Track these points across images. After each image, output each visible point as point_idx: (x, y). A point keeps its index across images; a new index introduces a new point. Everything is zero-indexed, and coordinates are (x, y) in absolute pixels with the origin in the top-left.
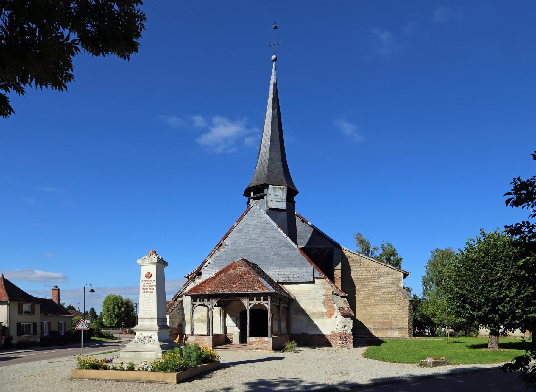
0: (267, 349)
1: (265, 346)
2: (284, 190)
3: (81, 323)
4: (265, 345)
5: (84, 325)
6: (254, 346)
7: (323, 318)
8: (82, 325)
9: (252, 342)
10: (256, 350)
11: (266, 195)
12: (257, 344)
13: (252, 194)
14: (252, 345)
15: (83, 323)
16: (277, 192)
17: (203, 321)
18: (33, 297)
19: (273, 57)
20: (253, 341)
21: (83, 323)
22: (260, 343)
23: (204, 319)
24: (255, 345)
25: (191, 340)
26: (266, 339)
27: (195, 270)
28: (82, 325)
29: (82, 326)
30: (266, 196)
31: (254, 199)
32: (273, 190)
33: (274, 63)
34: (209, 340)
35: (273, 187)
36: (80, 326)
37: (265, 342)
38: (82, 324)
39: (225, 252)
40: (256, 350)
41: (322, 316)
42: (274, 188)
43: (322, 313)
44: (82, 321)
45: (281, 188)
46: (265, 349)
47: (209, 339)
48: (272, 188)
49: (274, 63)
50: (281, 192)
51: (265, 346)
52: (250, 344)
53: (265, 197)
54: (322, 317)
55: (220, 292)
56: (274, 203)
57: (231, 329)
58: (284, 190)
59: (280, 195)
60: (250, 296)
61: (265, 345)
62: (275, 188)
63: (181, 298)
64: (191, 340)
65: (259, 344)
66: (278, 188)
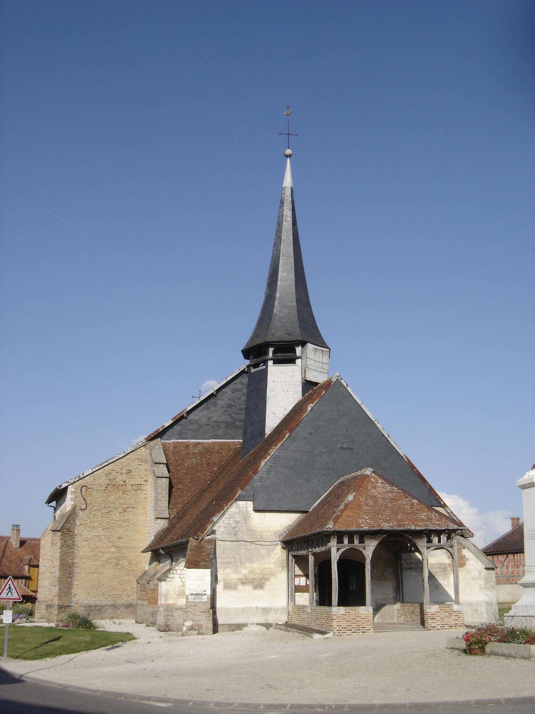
0: (457, 624)
1: (454, 620)
2: (326, 353)
3: (8, 586)
4: (454, 617)
5: (14, 591)
6: (439, 620)
7: (446, 573)
8: (10, 590)
9: (435, 614)
10: (441, 627)
11: (300, 358)
12: (442, 616)
13: (271, 350)
14: (435, 618)
15: (12, 586)
16: (318, 355)
17: (253, 581)
18: (524, 543)
19: (289, 152)
20: (437, 612)
21: (12, 586)
22: (447, 614)
23: (256, 577)
24: (438, 618)
25: (336, 615)
26: (361, 610)
27: (83, 474)
28: (10, 590)
29: (10, 594)
30: (300, 360)
31: (277, 362)
32: (313, 352)
33: (288, 160)
34: (368, 614)
35: (314, 348)
36: (6, 591)
37: (455, 614)
38: (10, 588)
39: (293, 455)
40: (441, 627)
41: (444, 571)
42: (315, 350)
43: (445, 564)
44: (10, 582)
45: (322, 350)
46: (454, 624)
47: (368, 611)
48: (312, 349)
49: (288, 160)
50: (323, 357)
51: (454, 620)
52: (432, 617)
53: (298, 362)
54: (444, 573)
55: (386, 526)
56: (314, 373)
57: (303, 597)
58: (326, 353)
59: (321, 361)
60: (340, 536)
61: (454, 617)
62: (316, 349)
63: (212, 536)
64: (336, 615)
65: (445, 617)
66: (319, 350)
